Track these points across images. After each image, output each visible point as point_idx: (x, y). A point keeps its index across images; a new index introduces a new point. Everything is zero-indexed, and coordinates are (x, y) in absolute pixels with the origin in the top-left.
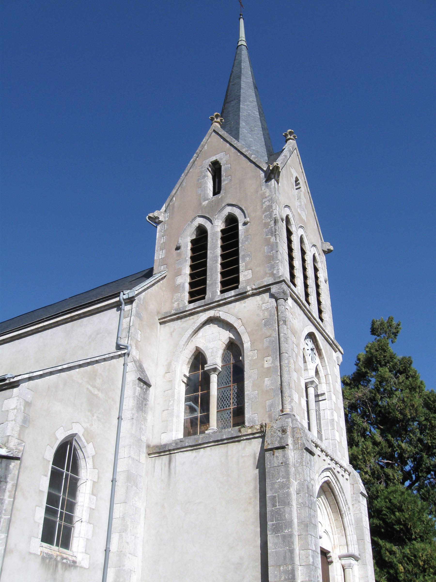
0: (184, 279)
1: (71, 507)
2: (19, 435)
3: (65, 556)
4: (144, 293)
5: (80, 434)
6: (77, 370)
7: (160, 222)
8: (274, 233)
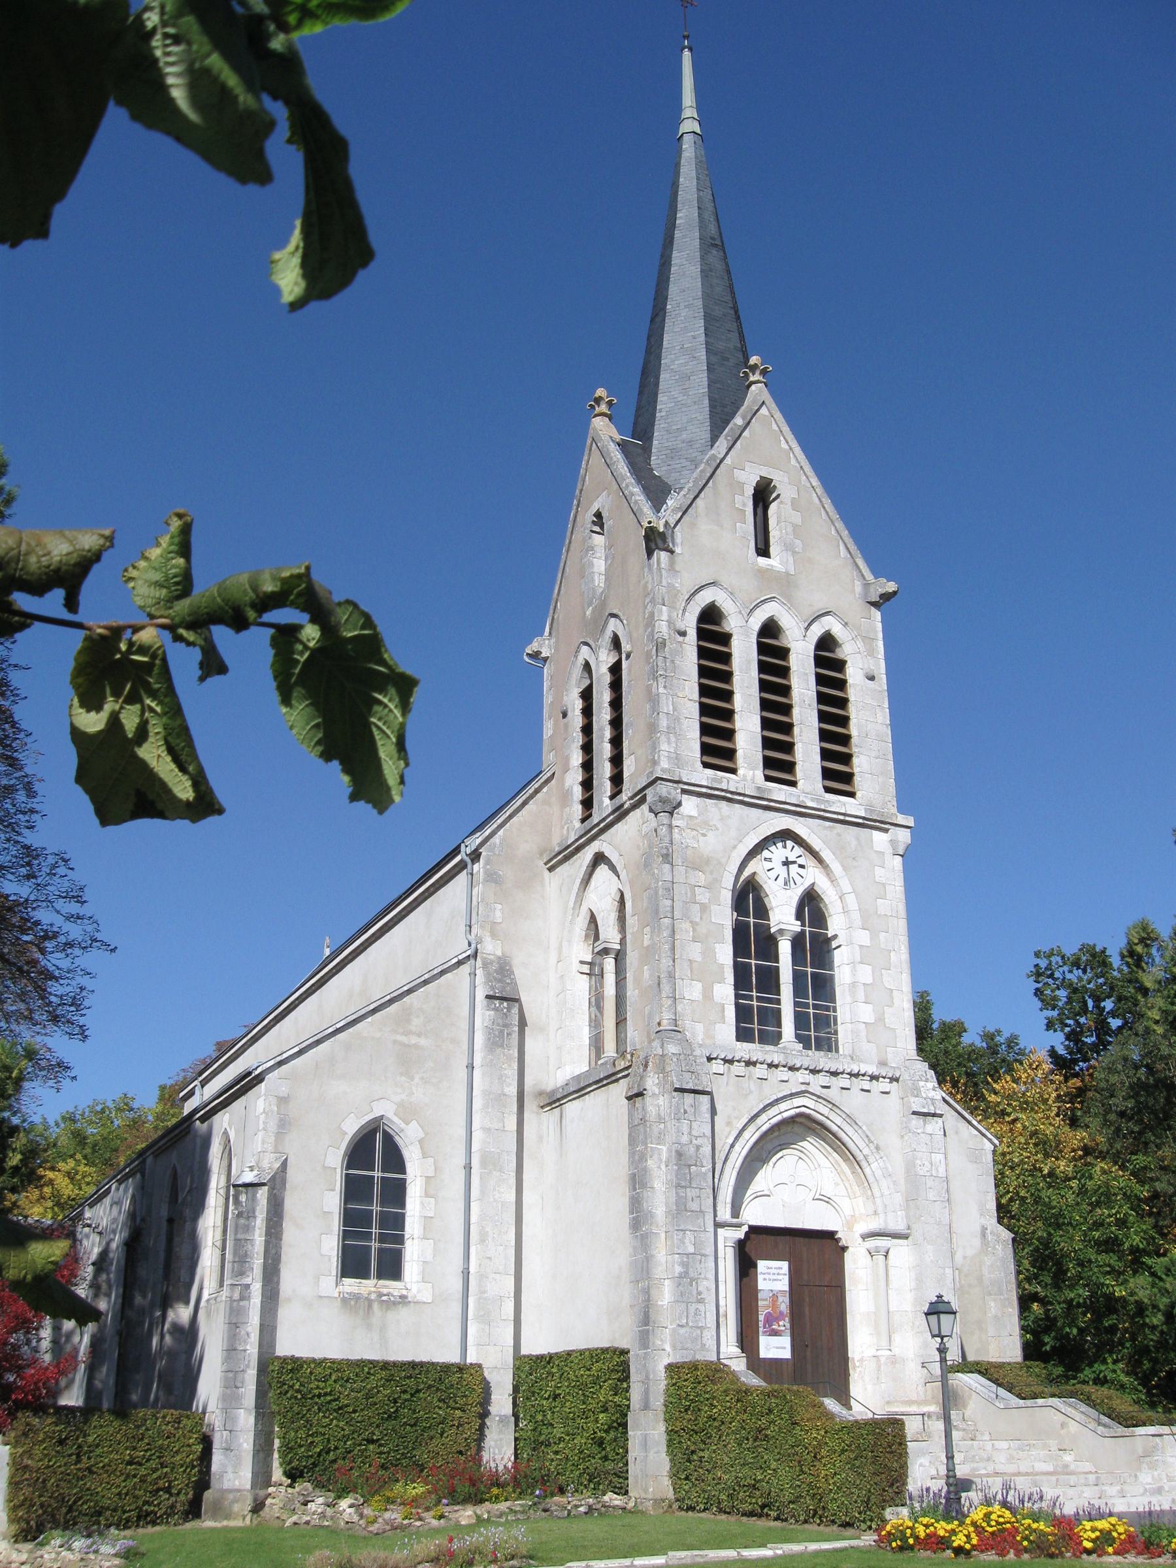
1: (398, 1222)
2: (276, 1146)
3: (385, 1291)
4: (501, 833)
5: (390, 1115)
6: (369, 1019)
7: (545, 659)
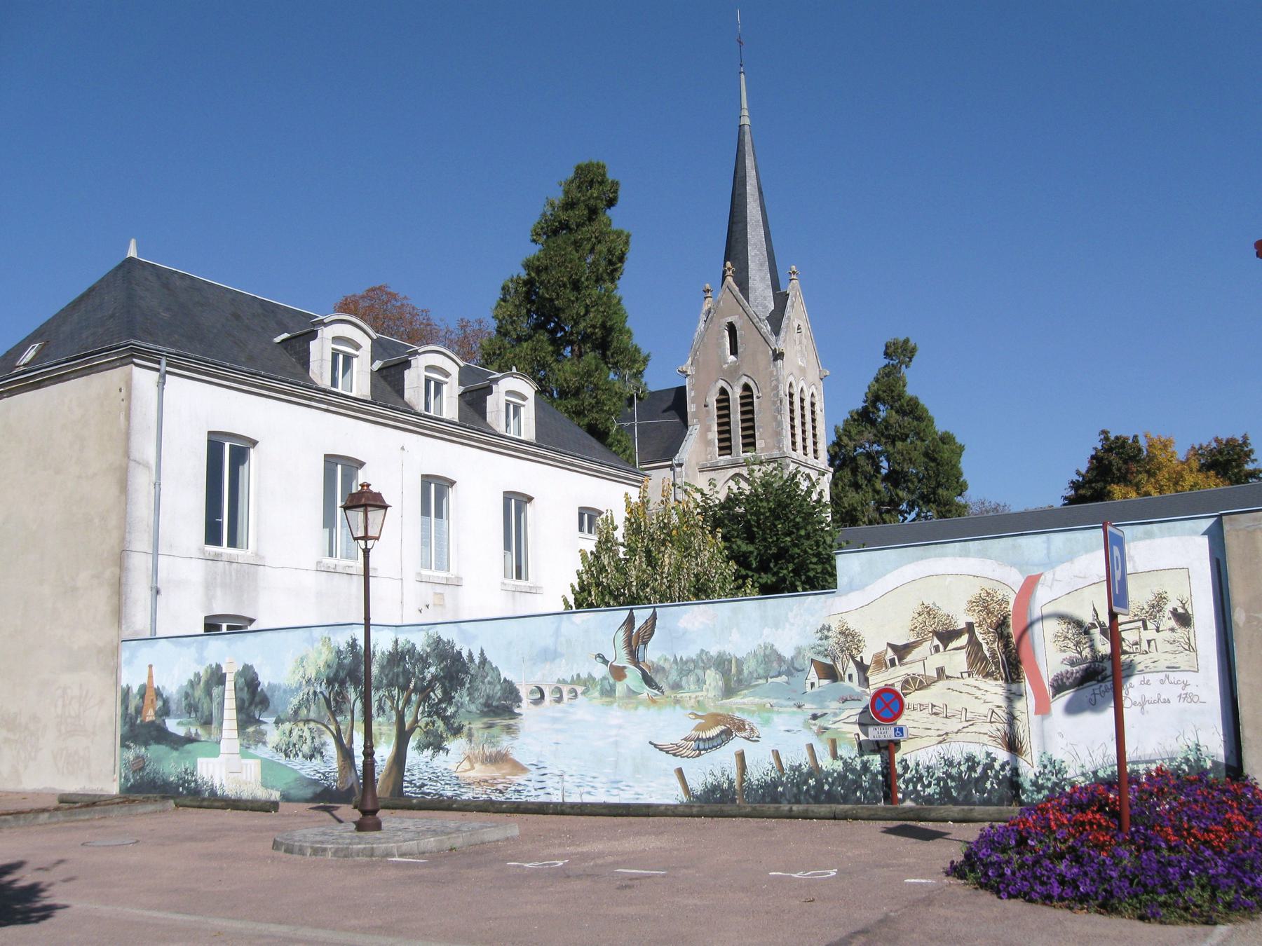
0: (714, 435)
8: (779, 411)
